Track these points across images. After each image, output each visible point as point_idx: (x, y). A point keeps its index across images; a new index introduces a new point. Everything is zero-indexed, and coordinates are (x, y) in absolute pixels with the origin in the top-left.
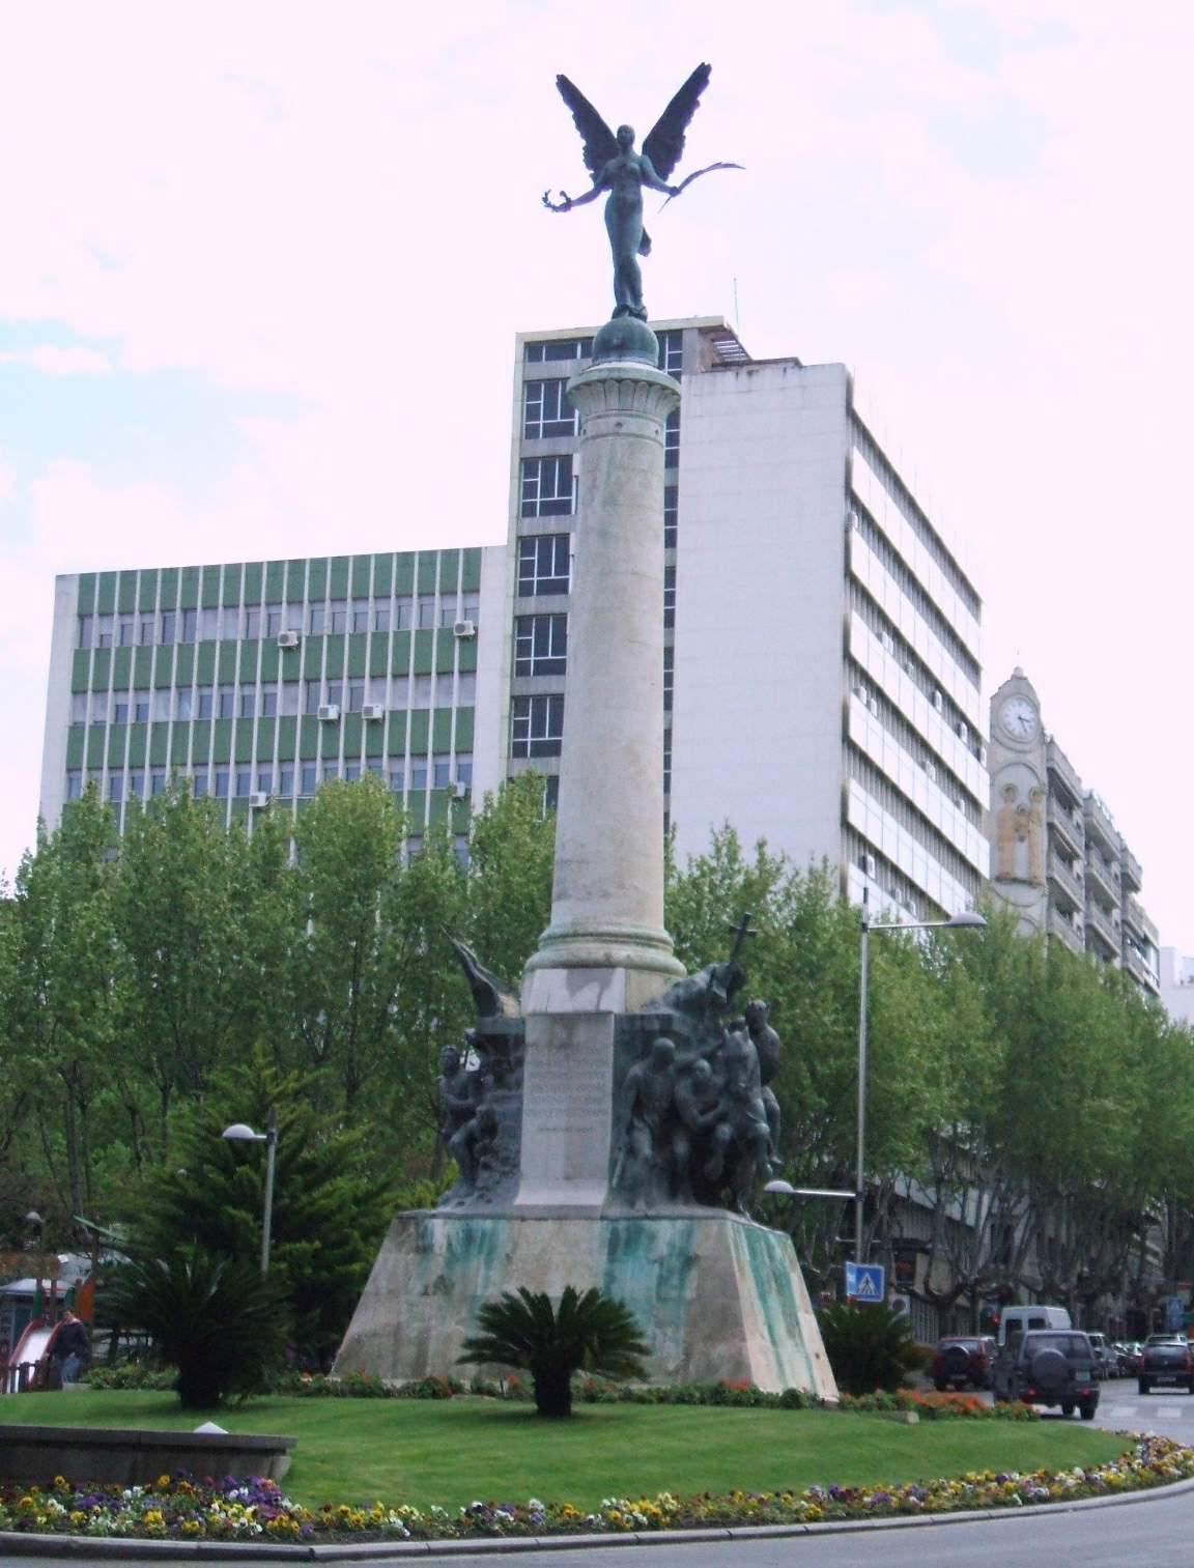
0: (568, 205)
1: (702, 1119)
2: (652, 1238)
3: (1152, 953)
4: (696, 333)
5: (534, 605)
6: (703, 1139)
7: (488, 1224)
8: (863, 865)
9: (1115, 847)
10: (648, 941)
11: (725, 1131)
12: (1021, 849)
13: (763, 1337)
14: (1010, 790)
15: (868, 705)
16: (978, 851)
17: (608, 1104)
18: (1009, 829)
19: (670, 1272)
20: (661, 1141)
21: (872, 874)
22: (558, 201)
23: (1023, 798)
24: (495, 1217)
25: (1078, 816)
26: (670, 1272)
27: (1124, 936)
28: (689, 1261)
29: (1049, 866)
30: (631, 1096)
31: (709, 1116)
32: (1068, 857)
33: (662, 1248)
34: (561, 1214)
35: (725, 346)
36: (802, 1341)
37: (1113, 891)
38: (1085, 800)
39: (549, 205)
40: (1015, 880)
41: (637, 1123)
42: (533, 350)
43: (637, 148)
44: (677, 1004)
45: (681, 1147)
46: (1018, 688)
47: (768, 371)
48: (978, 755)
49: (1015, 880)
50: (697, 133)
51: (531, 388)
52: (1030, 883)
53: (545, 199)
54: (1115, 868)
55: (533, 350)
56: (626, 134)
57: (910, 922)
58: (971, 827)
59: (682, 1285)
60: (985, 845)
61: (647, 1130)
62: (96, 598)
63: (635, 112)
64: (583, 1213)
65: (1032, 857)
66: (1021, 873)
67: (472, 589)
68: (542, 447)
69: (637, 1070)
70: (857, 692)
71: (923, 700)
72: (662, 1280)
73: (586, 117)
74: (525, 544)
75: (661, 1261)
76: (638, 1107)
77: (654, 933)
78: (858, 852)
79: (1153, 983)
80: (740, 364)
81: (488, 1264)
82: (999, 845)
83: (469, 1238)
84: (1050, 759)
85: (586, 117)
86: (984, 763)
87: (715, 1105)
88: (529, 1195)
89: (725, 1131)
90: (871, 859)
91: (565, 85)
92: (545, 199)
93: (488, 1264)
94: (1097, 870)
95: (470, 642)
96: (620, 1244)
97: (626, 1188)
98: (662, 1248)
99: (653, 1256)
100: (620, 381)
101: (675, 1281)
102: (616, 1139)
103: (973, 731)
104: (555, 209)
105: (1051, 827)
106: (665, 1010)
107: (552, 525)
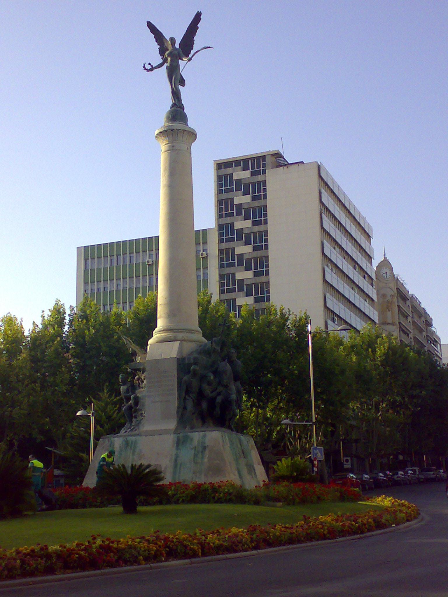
0: (152, 69)
1: (211, 395)
2: (192, 440)
3: (439, 345)
4: (270, 156)
5: (224, 246)
6: (212, 402)
7: (133, 438)
8: (333, 320)
9: (422, 312)
10: (191, 331)
11: (219, 399)
12: (389, 314)
13: (235, 475)
14: (384, 296)
15: (332, 270)
16: (374, 315)
17: (176, 391)
18: (384, 307)
19: (198, 452)
20: (198, 403)
21: (336, 323)
22: (149, 67)
23: (389, 298)
24: (135, 435)
25: (408, 303)
26: (198, 452)
27: (428, 340)
28: (205, 448)
29: (399, 319)
30: (185, 387)
31: (214, 394)
32: (406, 317)
33: (195, 442)
34: (160, 433)
35: (280, 160)
36: (256, 476)
37: (423, 326)
38: (411, 298)
39: (145, 69)
40: (388, 324)
41: (187, 397)
42: (220, 166)
43: (177, 46)
44: (200, 353)
45: (204, 405)
46: (385, 263)
47: (293, 166)
48: (372, 285)
49: (388, 324)
50: (199, 41)
51: (219, 178)
52: (393, 324)
53: (144, 67)
54: (423, 319)
55: (220, 166)
56: (173, 40)
57: (346, 337)
58: (371, 308)
59: (203, 457)
60: (376, 313)
61: (191, 400)
62: (77, 248)
63: (175, 32)
64: (166, 432)
65: (393, 315)
66: (390, 321)
67: (205, 243)
68: (224, 196)
69: (186, 378)
70: (328, 266)
71: (351, 268)
72: (195, 456)
73: (158, 36)
74: (220, 227)
75: (195, 448)
76: (187, 392)
77: (193, 328)
78: (331, 315)
79: (440, 355)
80: (285, 165)
81: (133, 454)
82: (382, 313)
83: (127, 443)
84: (397, 284)
85: (158, 36)
86: (374, 287)
87: (216, 389)
88: (146, 427)
89: (219, 399)
90: (336, 318)
91: (150, 25)
92: (144, 67)
93: (133, 454)
94: (416, 319)
95: (205, 258)
96: (179, 443)
97: (183, 421)
98: (195, 442)
99: (192, 447)
100: (172, 130)
101: (200, 455)
102: (179, 403)
103: (370, 277)
104: (148, 71)
105: (399, 306)
106: (195, 355)
107: (228, 220)
